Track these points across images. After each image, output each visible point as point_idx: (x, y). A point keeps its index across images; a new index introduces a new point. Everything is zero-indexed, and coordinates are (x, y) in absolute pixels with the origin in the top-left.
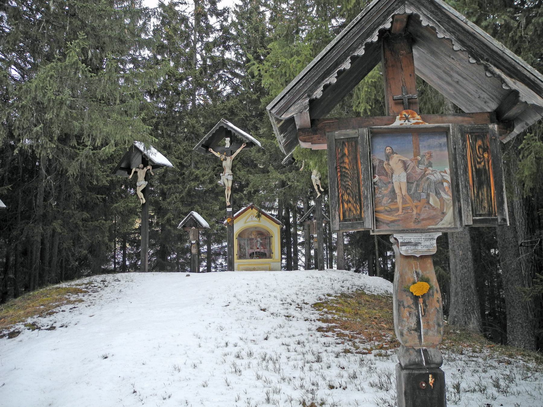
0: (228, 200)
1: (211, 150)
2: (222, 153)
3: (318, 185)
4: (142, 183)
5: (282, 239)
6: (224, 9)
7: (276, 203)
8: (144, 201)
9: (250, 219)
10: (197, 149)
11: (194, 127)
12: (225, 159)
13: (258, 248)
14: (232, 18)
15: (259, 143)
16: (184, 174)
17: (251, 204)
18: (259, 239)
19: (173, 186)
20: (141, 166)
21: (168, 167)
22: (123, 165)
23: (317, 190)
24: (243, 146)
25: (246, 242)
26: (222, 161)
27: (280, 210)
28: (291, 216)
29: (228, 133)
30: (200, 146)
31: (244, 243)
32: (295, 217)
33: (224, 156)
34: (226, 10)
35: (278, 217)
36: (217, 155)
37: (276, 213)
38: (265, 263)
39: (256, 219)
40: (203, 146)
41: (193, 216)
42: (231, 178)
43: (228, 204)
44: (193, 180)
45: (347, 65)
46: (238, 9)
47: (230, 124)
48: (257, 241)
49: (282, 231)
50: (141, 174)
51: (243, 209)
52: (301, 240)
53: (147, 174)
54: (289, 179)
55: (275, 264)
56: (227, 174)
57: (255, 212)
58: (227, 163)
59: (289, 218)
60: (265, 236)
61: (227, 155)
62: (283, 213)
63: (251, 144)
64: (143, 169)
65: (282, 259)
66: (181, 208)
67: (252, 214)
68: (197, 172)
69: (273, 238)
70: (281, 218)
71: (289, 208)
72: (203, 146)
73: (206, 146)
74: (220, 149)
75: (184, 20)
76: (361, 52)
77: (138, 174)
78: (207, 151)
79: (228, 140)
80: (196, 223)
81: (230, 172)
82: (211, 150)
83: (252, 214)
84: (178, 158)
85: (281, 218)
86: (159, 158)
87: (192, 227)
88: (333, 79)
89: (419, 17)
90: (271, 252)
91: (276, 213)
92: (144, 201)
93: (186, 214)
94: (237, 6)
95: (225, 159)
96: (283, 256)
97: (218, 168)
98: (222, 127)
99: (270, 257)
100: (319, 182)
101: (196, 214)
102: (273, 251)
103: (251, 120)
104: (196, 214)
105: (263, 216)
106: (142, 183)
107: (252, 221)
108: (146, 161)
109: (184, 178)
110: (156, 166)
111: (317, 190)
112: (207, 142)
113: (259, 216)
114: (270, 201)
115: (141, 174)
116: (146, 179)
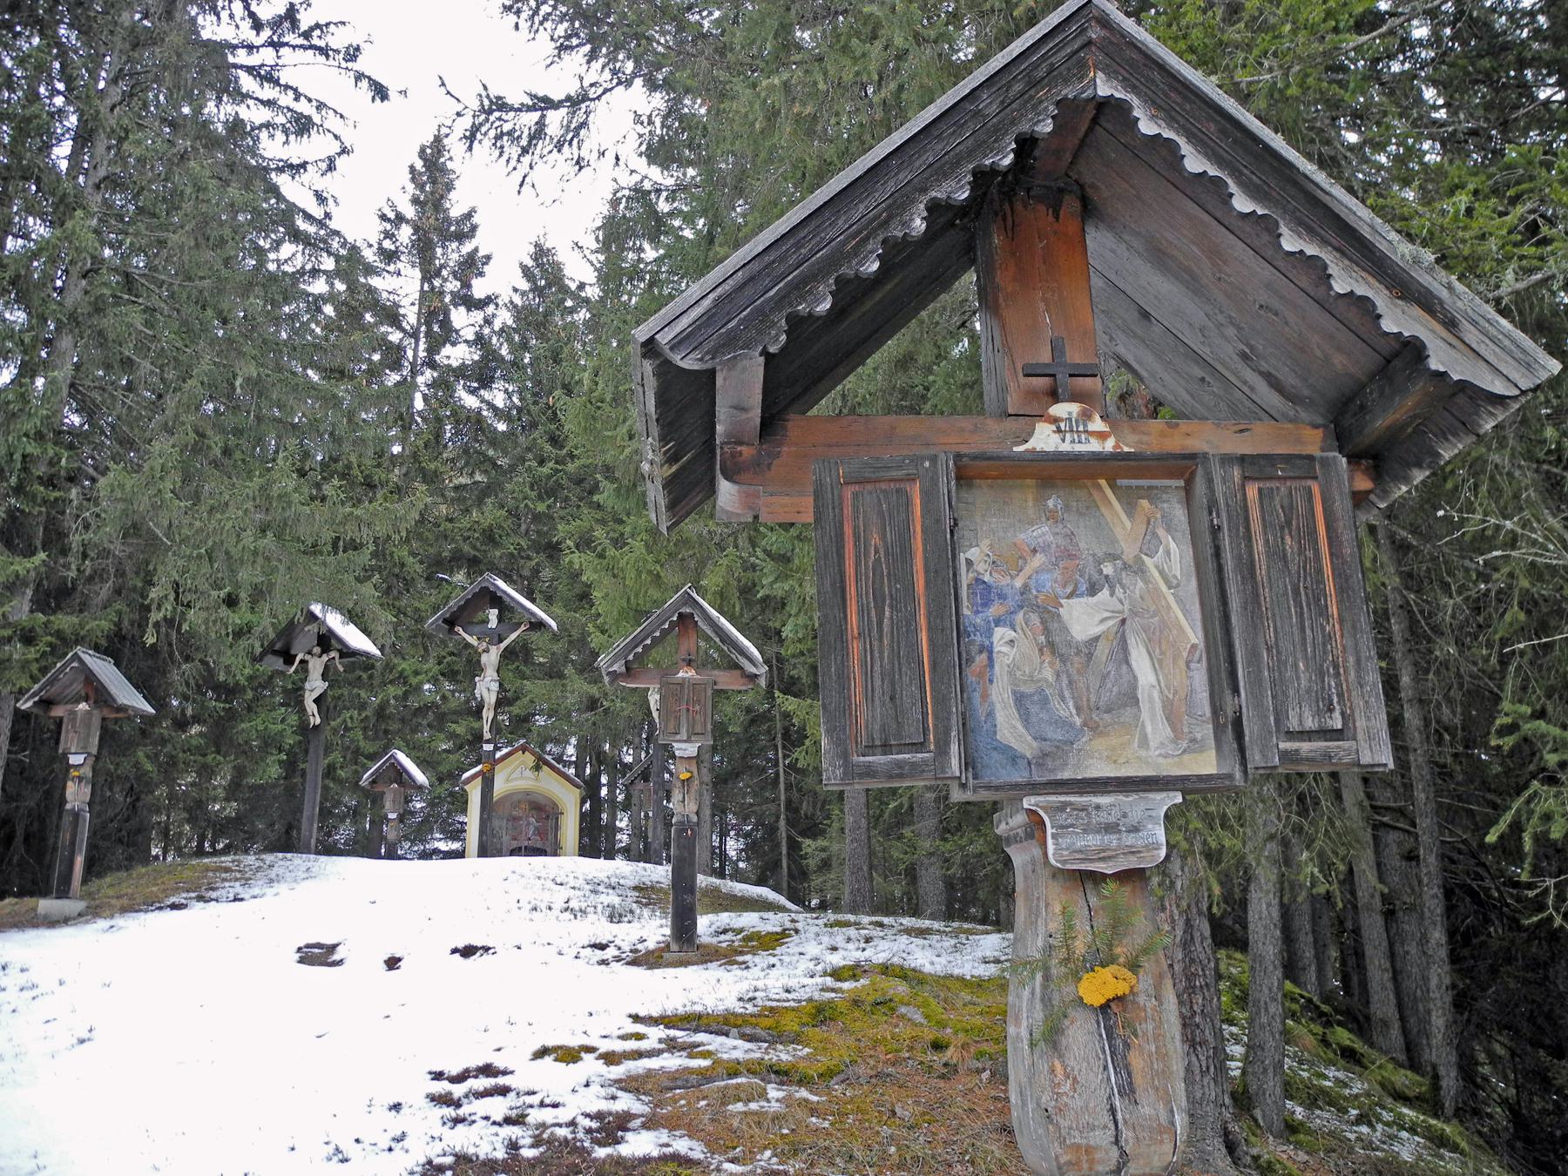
0: (486, 728)
1: (459, 629)
4: (316, 685)
6: (489, 297)
7: (571, 750)
8: (318, 721)
9: (517, 774)
11: (403, 565)
12: (487, 651)
14: (504, 318)
15: (553, 624)
18: (532, 820)
20: (317, 650)
21: (367, 655)
22: (277, 647)
24: (523, 628)
29: (496, 600)
32: (612, 786)
34: (488, 300)
36: (472, 640)
39: (528, 773)
40: (445, 621)
42: (495, 687)
43: (487, 736)
44: (391, 682)
45: (648, 641)
46: (518, 300)
47: (501, 583)
50: (316, 666)
53: (326, 667)
57: (529, 759)
58: (491, 658)
59: (600, 786)
60: (546, 812)
63: (539, 625)
66: (362, 744)
67: (523, 762)
68: (404, 665)
71: (600, 759)
72: (445, 621)
73: (451, 622)
75: (392, 316)
76: (657, 634)
77: (310, 665)
78: (451, 631)
79: (493, 614)
80: (399, 774)
82: (459, 629)
83: (523, 762)
86: (355, 638)
88: (640, 649)
89: (1130, 108)
92: (318, 721)
93: (373, 757)
94: (516, 290)
97: (449, 659)
98: (486, 588)
101: (401, 757)
103: (529, 558)
104: (401, 757)
105: (545, 768)
106: (316, 685)
107: (522, 778)
108: (326, 640)
109: (371, 677)
110: (347, 652)
112: (453, 614)
113: (537, 768)
114: (557, 742)
115: (316, 666)
116: (324, 677)
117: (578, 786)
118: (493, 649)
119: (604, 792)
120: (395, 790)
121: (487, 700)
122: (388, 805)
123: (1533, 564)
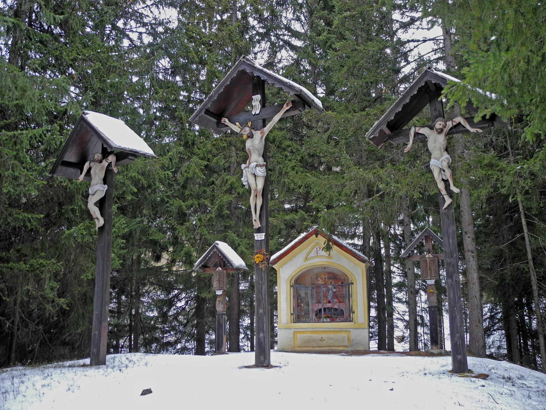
2: (243, 125)
3: (446, 182)
5: (369, 279)
9: (313, 254)
10: (197, 119)
12: (251, 136)
13: (329, 302)
16: (213, 183)
17: (315, 227)
19: (196, 202)
23: (444, 192)
24: (286, 108)
25: (309, 292)
26: (244, 142)
27: (365, 238)
28: (382, 246)
30: (203, 113)
31: (306, 294)
32: (387, 248)
33: (247, 129)
35: (363, 249)
36: (236, 128)
37: (360, 243)
38: (341, 330)
39: (324, 253)
41: (217, 249)
42: (261, 172)
48: (328, 290)
49: (369, 270)
51: (303, 235)
52: (396, 279)
53: (108, 171)
54: (381, 179)
55: (358, 331)
56: (253, 164)
57: (322, 240)
59: (380, 249)
61: (254, 128)
62: (372, 241)
64: (101, 162)
65: (369, 307)
69: (354, 286)
70: (367, 250)
71: (379, 235)
74: (243, 117)
80: (224, 262)
81: (261, 161)
82: (225, 121)
83: (317, 244)
84: (203, 159)
85: (367, 250)
87: (217, 267)
90: (351, 311)
91: (360, 243)
95: (251, 136)
96: (372, 304)
98: (243, 72)
99: (349, 319)
100: (448, 174)
101: (224, 247)
102: (354, 309)
104: (224, 247)
105: (335, 247)
107: (317, 256)
111: (444, 192)
113: (328, 248)
116: (105, 181)
117: (363, 261)
118: (257, 135)
119: (383, 251)
120: (219, 273)
121: (253, 186)
122: (215, 284)
123: (202, 266)
